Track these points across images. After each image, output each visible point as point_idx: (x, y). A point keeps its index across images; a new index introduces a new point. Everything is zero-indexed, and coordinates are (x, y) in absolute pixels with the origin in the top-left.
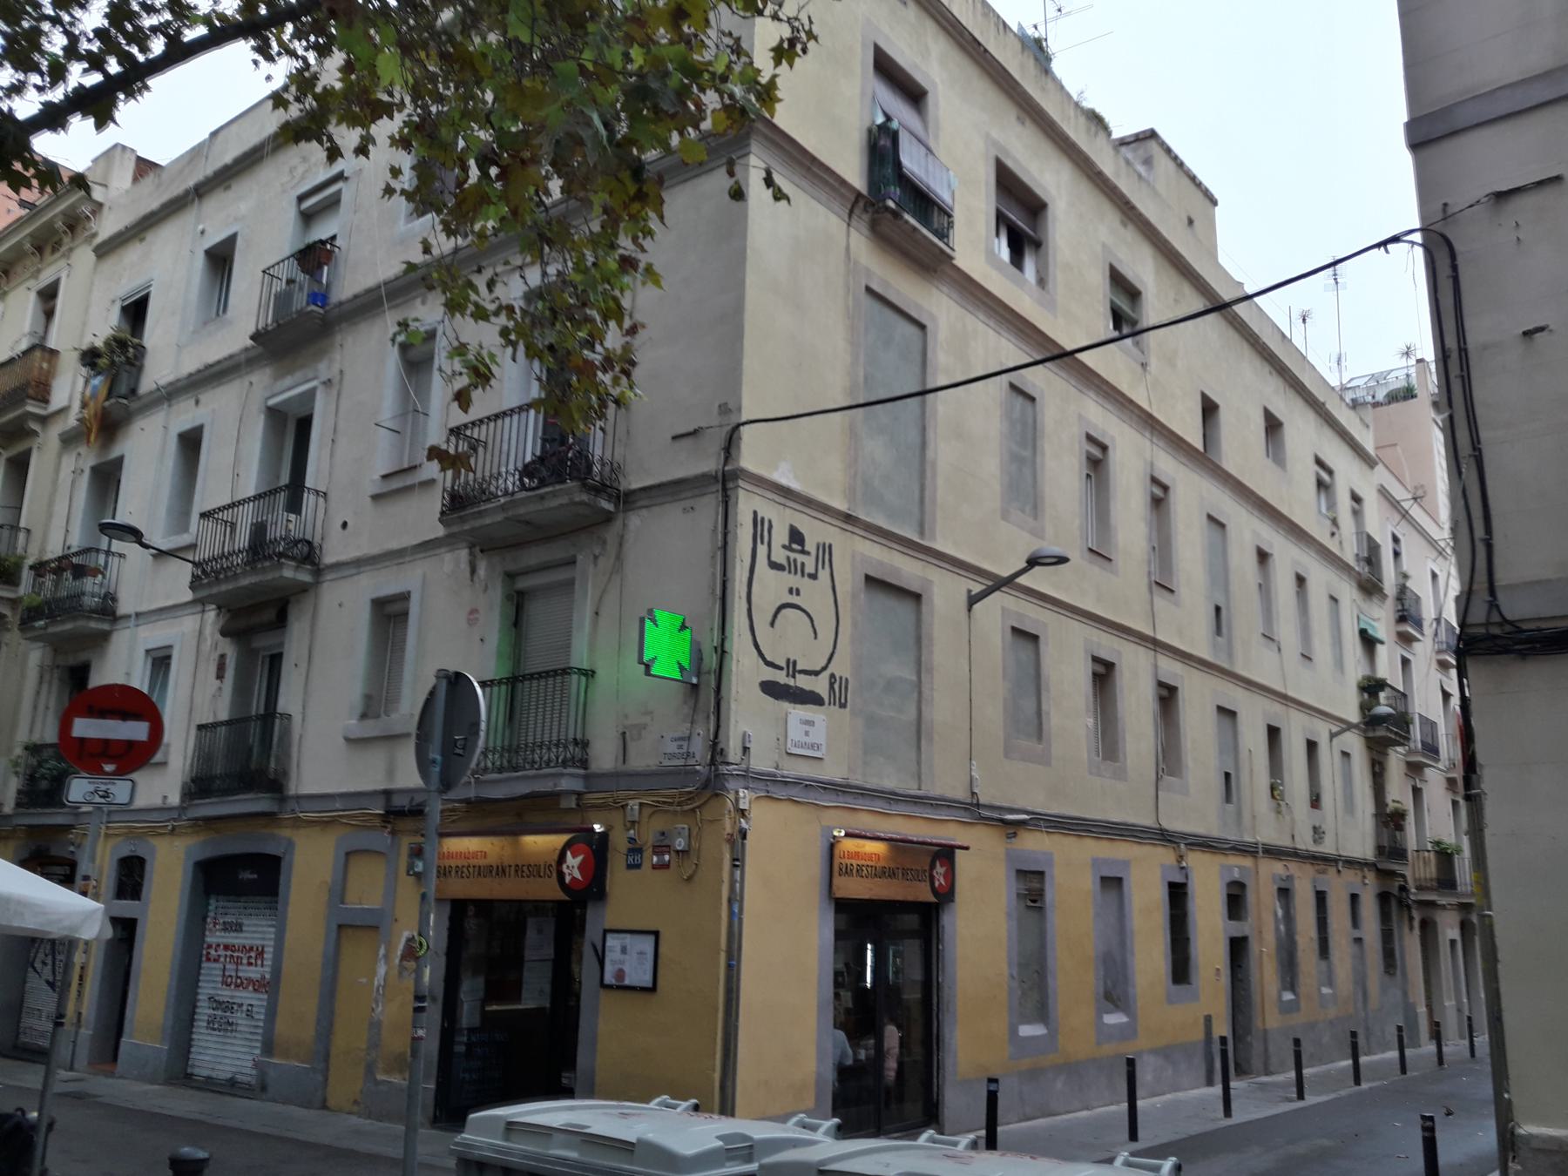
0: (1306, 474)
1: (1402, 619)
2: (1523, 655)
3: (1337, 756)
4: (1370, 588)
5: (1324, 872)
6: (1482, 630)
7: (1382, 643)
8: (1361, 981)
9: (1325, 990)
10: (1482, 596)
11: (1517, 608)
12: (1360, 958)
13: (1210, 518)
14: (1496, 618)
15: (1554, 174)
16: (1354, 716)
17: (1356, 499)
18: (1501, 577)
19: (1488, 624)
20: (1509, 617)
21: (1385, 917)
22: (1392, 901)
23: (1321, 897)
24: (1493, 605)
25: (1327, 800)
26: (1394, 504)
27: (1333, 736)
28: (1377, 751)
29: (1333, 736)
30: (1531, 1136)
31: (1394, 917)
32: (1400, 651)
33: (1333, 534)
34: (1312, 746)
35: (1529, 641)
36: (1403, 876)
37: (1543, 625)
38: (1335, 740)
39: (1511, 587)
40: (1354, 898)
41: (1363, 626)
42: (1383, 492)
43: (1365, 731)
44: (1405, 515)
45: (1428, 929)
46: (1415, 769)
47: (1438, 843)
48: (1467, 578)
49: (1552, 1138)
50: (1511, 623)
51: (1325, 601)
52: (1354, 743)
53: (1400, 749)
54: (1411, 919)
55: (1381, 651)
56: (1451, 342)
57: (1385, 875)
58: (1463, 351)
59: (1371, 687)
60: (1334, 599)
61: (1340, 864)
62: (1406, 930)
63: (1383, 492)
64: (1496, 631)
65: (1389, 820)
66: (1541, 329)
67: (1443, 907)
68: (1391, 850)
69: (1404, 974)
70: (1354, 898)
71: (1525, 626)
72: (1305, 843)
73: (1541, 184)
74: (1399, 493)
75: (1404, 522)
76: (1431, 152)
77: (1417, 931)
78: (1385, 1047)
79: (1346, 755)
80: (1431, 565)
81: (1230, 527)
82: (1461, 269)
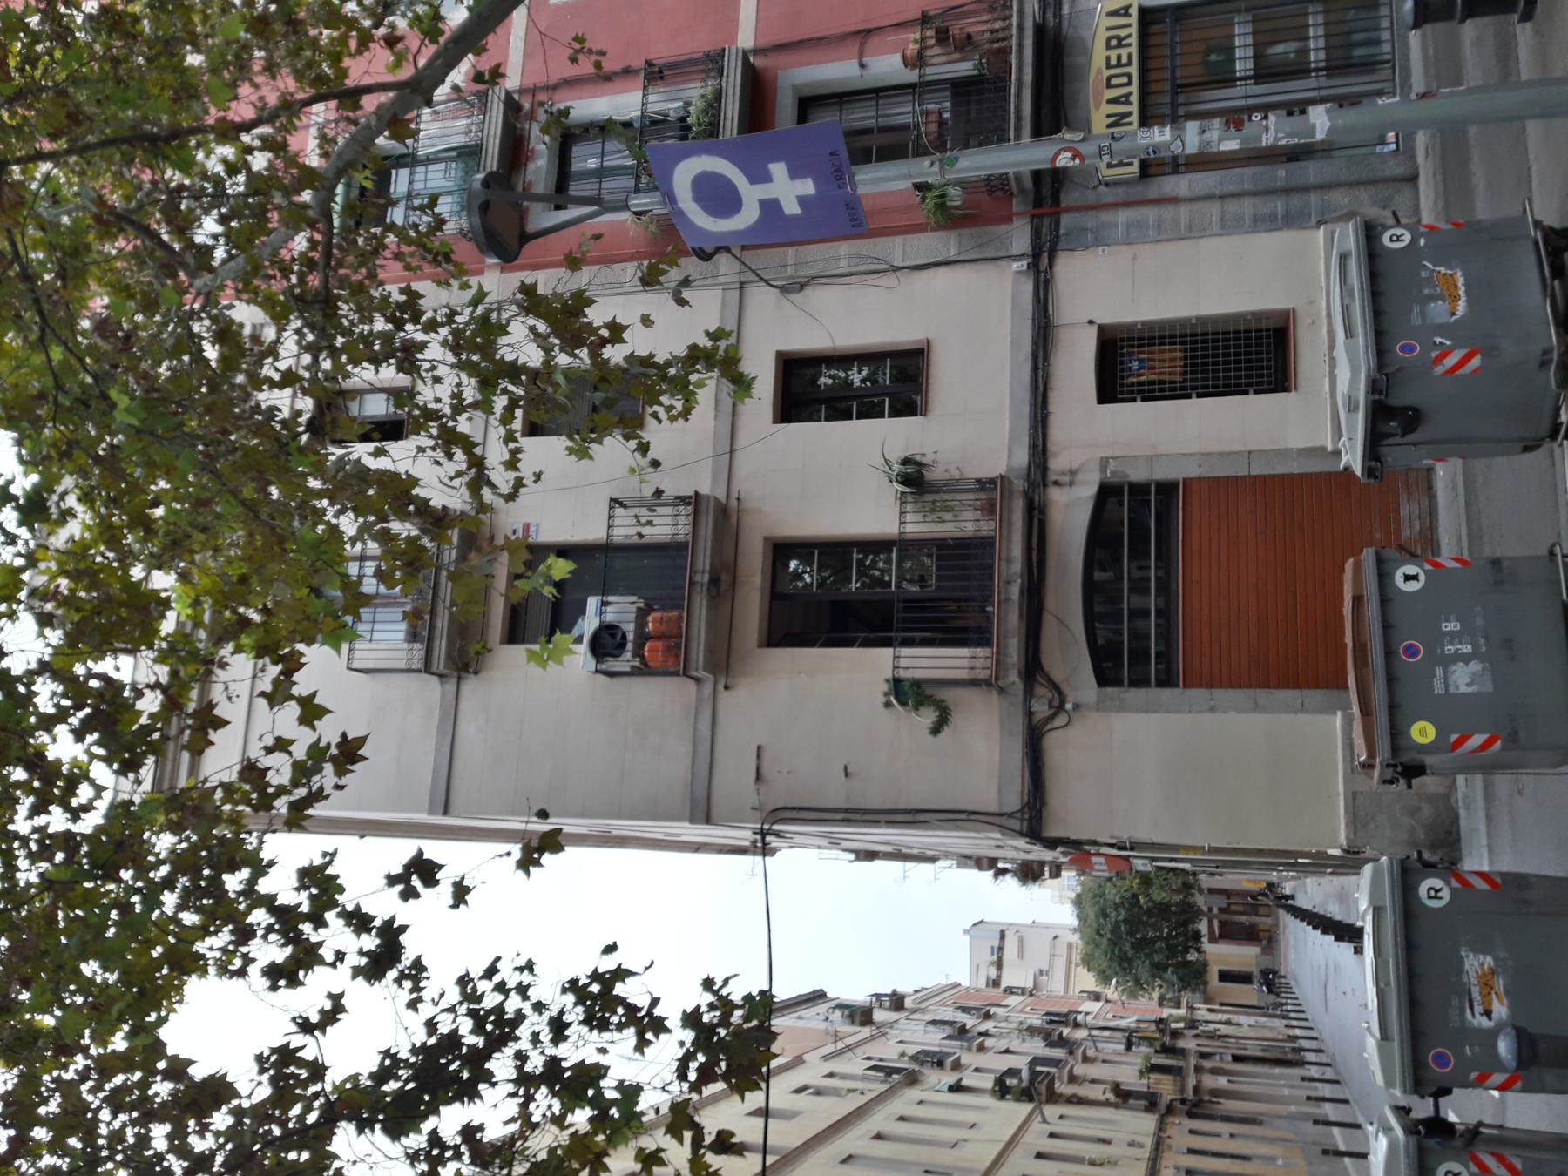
0: (803, 1101)
1: (940, 1064)
2: (1043, 803)
3: (1061, 1122)
4: (912, 1079)
5: (1170, 1147)
6: (1025, 823)
7: (961, 1079)
8: (1272, 1140)
9: (1280, 1162)
10: (1004, 821)
11: (1014, 802)
12: (1247, 1137)
13: (844, 1161)
14: (1018, 815)
15: (755, 750)
16: (1025, 1108)
17: (831, 1075)
18: (994, 808)
19: (1022, 820)
20: (1019, 807)
21: (1210, 1117)
22: (1197, 1107)
23: (1191, 1151)
24: (1010, 815)
25: (1103, 1134)
26: (837, 1054)
27: (1044, 1121)
28: (1053, 1098)
29: (1044, 1121)
30: (1347, 837)
31: (1208, 1112)
32: (969, 1071)
33: (862, 1093)
34: (1052, 1135)
35: (1035, 800)
36: (1172, 1101)
37: (1026, 790)
38: (1049, 1120)
39: (1000, 804)
40: (1191, 1132)
41: (946, 1088)
42: (827, 1058)
43: (1040, 1102)
44: (849, 1048)
45: (1216, 1093)
46: (1073, 1079)
47: (1141, 1073)
48: (990, 827)
49: (1347, 826)
50: (1023, 808)
51: (921, 1107)
52: (1051, 1111)
53: (1057, 1085)
54: (1210, 1102)
55: (965, 1082)
56: (840, 816)
57: (1170, 1110)
58: (846, 811)
59: (1001, 1089)
60: (921, 1102)
61: (1162, 1134)
62: (1219, 1106)
63: (827, 1058)
64: (1026, 816)
65: (1123, 1096)
66: (846, 768)
67: (1199, 1082)
68: (1150, 1102)
69: (1262, 1114)
70: (1191, 1132)
71: (1026, 799)
72: (1145, 1153)
73: (758, 756)
74: (830, 1048)
75: (856, 1051)
76: (716, 810)
77: (1222, 1101)
78: (1331, 1135)
79: (1061, 1117)
80: (892, 1042)
81: (852, 1151)
82: (795, 805)
